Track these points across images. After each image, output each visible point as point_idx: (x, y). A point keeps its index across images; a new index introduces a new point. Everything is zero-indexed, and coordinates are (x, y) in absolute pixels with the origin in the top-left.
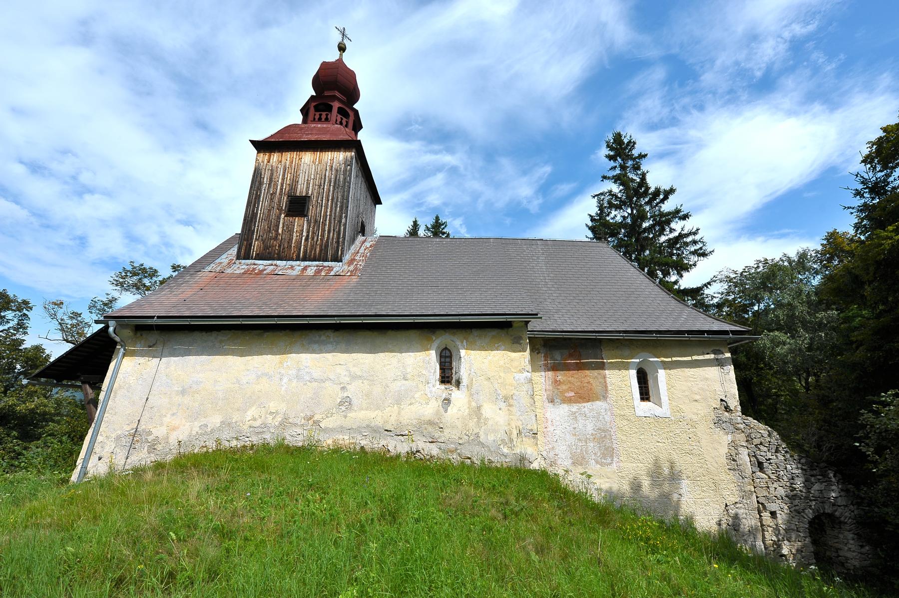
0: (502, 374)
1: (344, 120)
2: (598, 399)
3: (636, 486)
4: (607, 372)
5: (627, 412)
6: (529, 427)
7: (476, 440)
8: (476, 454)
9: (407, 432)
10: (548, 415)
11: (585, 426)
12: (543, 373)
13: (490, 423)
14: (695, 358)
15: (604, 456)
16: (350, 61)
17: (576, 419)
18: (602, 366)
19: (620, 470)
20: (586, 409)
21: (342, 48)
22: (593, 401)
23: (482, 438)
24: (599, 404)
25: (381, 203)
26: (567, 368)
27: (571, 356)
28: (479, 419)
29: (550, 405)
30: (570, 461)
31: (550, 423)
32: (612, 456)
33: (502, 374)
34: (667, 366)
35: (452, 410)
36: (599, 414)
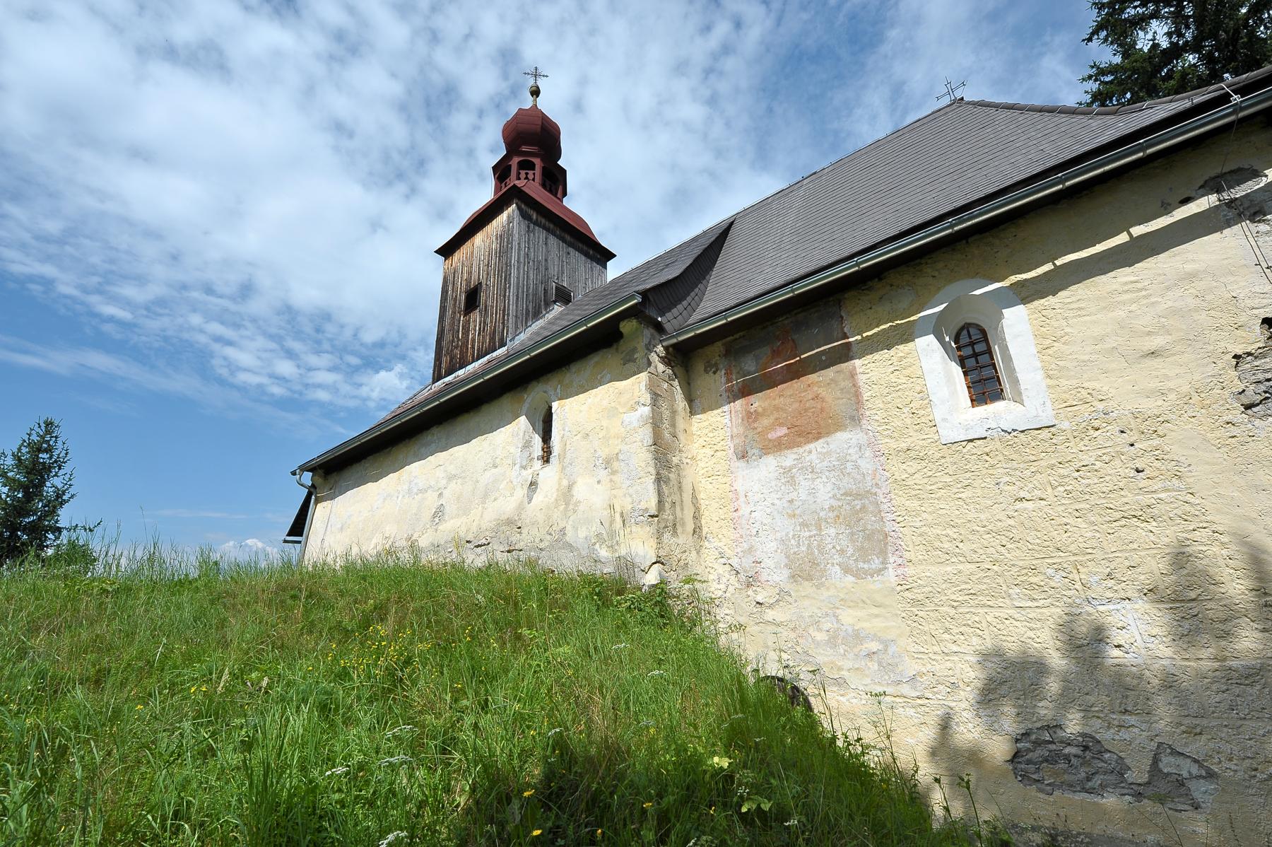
0: (605, 423)
1: (531, 172)
2: (839, 427)
3: (1087, 644)
4: (857, 362)
5: (914, 439)
6: (643, 505)
7: (560, 541)
8: (566, 564)
9: (484, 541)
10: (738, 486)
11: (813, 492)
12: (726, 408)
13: (581, 508)
14: (1137, 231)
15: (863, 554)
16: (544, 104)
17: (792, 481)
18: (845, 354)
19: (905, 585)
20: (814, 456)
21: (536, 92)
22: (828, 434)
23: (570, 537)
24: (842, 440)
25: (611, 256)
26: (768, 382)
27: (777, 355)
28: (567, 504)
29: (742, 463)
30: (786, 573)
31: (742, 499)
32: (883, 553)
33: (605, 423)
34: (1025, 293)
35: (538, 498)
36: (843, 460)
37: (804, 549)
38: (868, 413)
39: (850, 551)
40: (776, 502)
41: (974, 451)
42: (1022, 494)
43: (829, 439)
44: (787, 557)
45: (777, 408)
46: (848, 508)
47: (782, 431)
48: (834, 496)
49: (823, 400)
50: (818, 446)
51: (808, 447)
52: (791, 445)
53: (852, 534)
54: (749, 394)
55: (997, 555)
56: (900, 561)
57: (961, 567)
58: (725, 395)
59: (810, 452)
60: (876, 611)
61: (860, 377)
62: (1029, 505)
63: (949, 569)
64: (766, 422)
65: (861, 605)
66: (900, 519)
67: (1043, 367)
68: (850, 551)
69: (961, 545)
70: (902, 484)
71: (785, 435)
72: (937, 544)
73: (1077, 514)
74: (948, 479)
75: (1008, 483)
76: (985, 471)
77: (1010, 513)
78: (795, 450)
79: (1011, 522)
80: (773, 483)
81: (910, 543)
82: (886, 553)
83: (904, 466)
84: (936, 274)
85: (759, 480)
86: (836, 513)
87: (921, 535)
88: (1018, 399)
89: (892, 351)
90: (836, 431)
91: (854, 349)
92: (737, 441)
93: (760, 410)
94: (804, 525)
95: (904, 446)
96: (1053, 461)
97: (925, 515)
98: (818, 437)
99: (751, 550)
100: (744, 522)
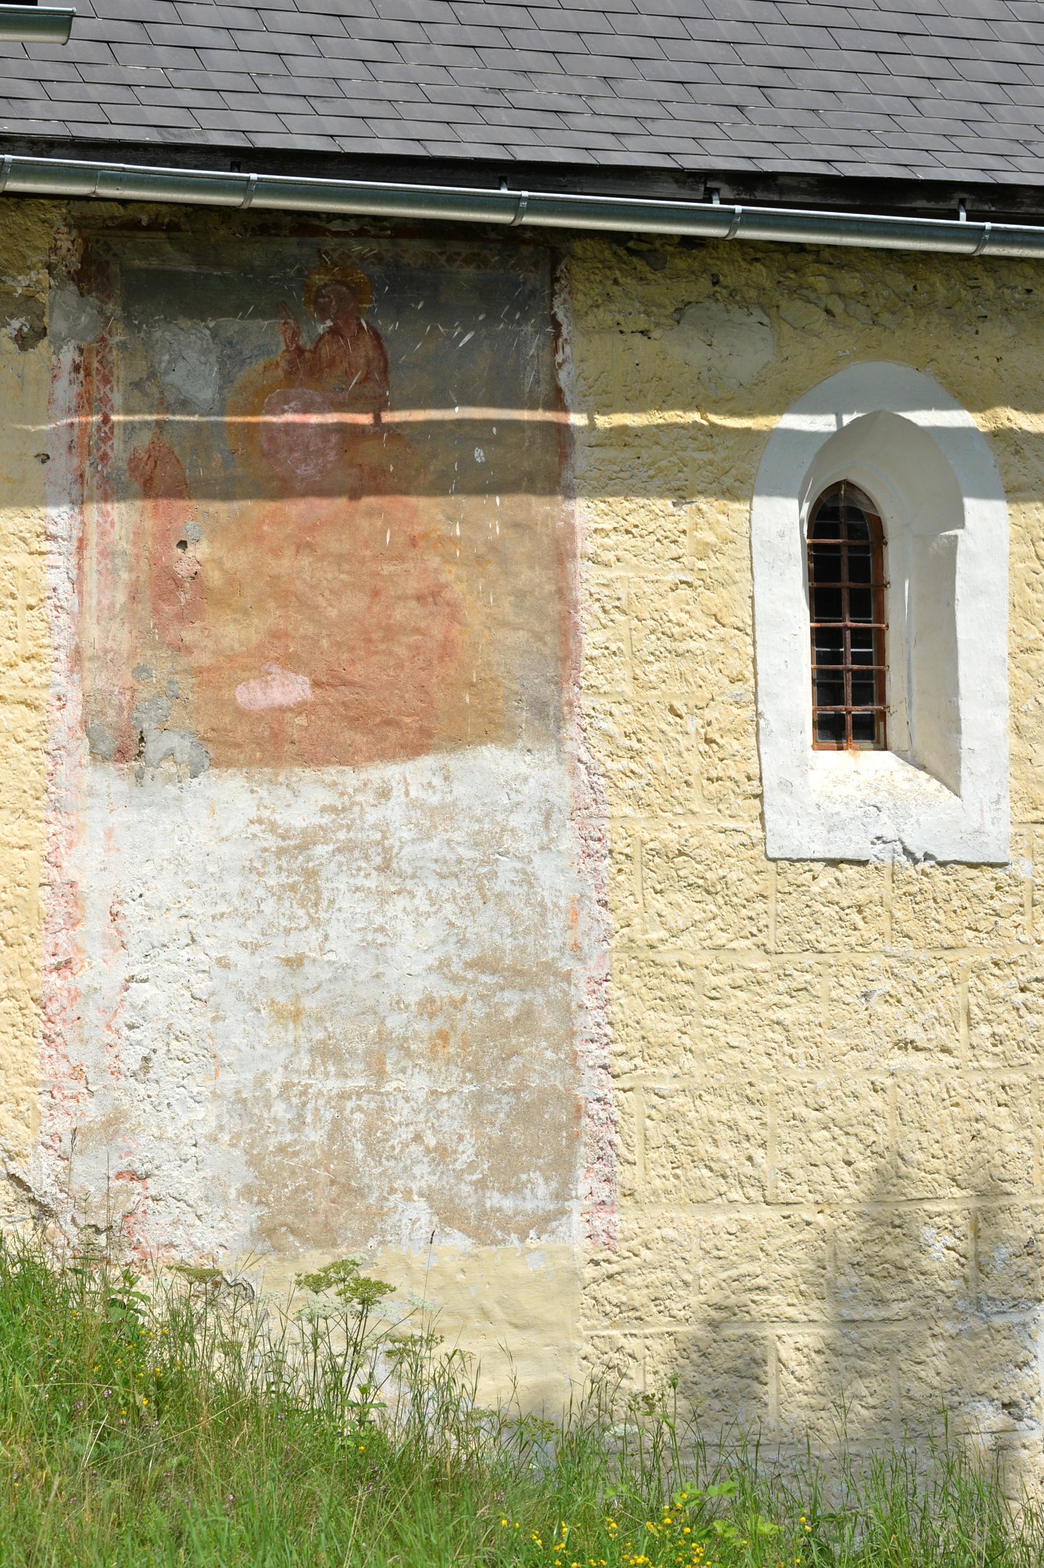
2: (494, 729)
4: (584, 512)
10: (84, 865)
11: (376, 943)
15: (504, 1166)
17: (307, 888)
18: (548, 466)
20: (394, 811)
22: (457, 742)
24: (500, 772)
26: (265, 472)
27: (305, 372)
29: (110, 780)
30: (245, 1217)
31: (96, 924)
32: (562, 1167)
36: (491, 844)
37: (315, 1135)
38: (586, 703)
39: (466, 1153)
40: (239, 957)
41: (835, 893)
42: (912, 1032)
43: (453, 762)
44: (255, 1162)
45: (282, 592)
46: (478, 1010)
47: (289, 689)
48: (444, 964)
49: (454, 613)
50: (413, 777)
51: (380, 773)
52: (319, 753)
53: (480, 1098)
54: (181, 489)
55: (831, 1188)
56: (603, 1191)
57: (748, 1215)
58: (63, 464)
59: (384, 794)
60: (515, 1340)
61: (583, 569)
62: (916, 1061)
63: (720, 1219)
64: (232, 633)
65: (475, 1323)
66: (622, 1064)
67: (1013, 700)
68: (466, 1153)
69: (758, 1154)
70: (644, 957)
71: (301, 708)
72: (705, 1147)
73: (1003, 1097)
74: (760, 963)
75: (889, 998)
76: (846, 956)
77: (880, 1079)
78: (331, 773)
79: (876, 1102)
80: (233, 884)
81: (637, 1140)
82: (571, 1167)
83: (658, 903)
84: (838, 307)
85: (179, 861)
86: (439, 1023)
87: (668, 1119)
88: (943, 765)
89: (684, 515)
90: (484, 737)
91: (582, 459)
92: (98, 680)
93: (215, 578)
94: (326, 1052)
95: (670, 838)
96: (985, 958)
97: (688, 1061)
98: (416, 747)
99: (113, 1125)
100: (92, 1015)
